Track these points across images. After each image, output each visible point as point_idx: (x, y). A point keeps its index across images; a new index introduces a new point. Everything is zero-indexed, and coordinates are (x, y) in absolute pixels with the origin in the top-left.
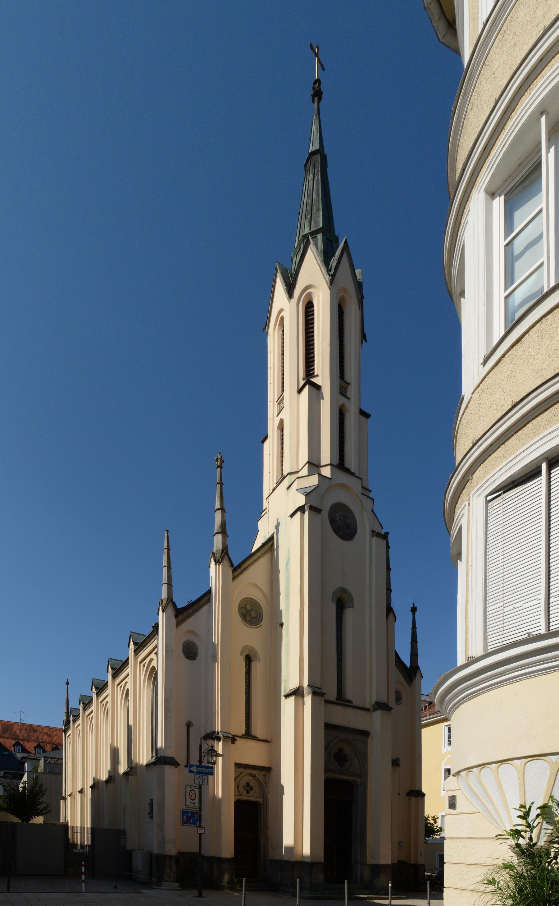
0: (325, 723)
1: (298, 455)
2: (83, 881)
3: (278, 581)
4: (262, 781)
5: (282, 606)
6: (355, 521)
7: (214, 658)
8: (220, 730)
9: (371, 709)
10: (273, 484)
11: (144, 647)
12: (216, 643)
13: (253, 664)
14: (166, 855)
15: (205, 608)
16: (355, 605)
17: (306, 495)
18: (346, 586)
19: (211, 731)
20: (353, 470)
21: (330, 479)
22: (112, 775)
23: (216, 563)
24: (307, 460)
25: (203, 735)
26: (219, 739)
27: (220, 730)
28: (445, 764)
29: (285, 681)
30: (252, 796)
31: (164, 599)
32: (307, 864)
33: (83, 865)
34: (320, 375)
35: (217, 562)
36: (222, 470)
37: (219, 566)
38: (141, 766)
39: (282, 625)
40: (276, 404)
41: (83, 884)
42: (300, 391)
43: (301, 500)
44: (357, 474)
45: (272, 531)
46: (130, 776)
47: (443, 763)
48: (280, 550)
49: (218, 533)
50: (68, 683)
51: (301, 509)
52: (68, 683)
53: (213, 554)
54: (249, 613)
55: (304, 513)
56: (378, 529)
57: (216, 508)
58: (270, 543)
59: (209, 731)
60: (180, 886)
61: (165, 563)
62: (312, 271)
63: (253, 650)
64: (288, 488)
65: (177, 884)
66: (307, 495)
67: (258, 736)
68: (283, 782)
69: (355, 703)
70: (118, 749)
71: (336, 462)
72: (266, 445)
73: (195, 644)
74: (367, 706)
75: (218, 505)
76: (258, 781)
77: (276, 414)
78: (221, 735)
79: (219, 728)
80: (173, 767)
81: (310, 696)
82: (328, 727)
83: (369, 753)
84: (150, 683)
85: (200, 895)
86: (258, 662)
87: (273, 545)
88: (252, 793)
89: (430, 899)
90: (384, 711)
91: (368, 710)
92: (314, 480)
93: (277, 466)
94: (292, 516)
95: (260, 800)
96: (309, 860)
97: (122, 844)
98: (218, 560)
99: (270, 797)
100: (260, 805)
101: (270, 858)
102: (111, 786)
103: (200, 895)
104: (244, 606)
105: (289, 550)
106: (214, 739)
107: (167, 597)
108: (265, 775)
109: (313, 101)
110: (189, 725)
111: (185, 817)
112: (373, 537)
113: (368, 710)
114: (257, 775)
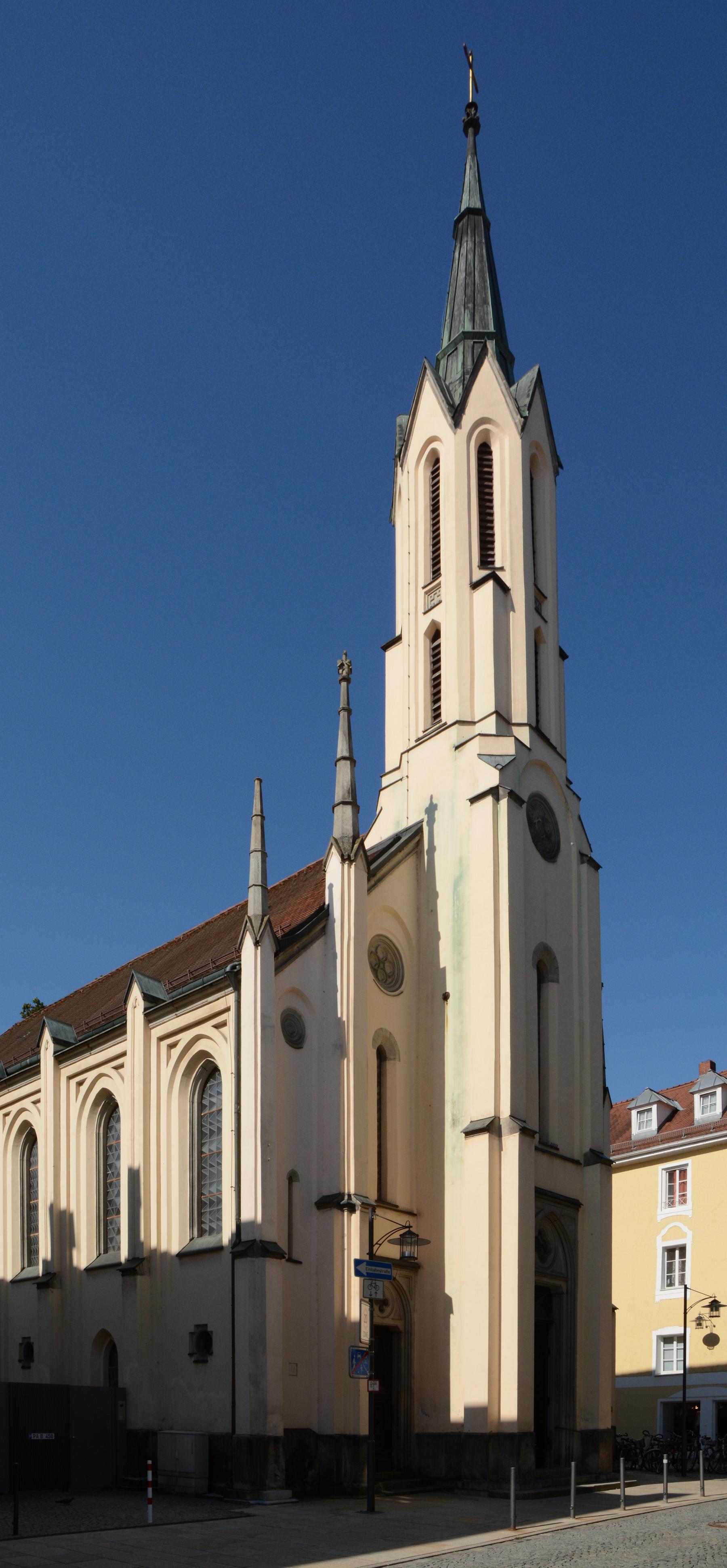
0: (536, 1188)
1: (471, 688)
2: (150, 1501)
3: (433, 912)
4: (405, 1288)
5: (446, 958)
6: (558, 830)
7: (340, 1049)
8: (352, 1191)
9: (582, 1161)
10: (417, 730)
11: (177, 1009)
12: (345, 1019)
13: (389, 1065)
14: (270, 1437)
15: (317, 947)
16: (561, 979)
17: (500, 770)
18: (551, 943)
19: (335, 1192)
20: (553, 741)
21: (529, 749)
22: (55, 1269)
23: (343, 860)
24: (493, 710)
25: (315, 1199)
26: (352, 1209)
27: (352, 1191)
28: (664, 1238)
29: (454, 1103)
30: (387, 1317)
31: (256, 916)
32: (510, 1436)
33: (148, 1467)
34: (507, 568)
35: (345, 858)
36: (350, 686)
37: (349, 867)
38: (165, 1254)
39: (446, 997)
40: (421, 592)
41: (150, 1507)
42: (475, 586)
43: (492, 778)
44: (558, 750)
45: (416, 815)
46: (139, 1277)
48: (437, 855)
49: (344, 803)
51: (493, 792)
53: (336, 840)
54: (382, 965)
55: (497, 799)
56: (586, 851)
57: (339, 756)
58: (417, 839)
59: (326, 1192)
60: (293, 1496)
61: (255, 843)
62: (489, 393)
63: (389, 1038)
64: (457, 748)
65: (288, 1493)
66: (502, 770)
67: (398, 1204)
68: (450, 1288)
69: (562, 1152)
70: (71, 1216)
71: (534, 724)
72: (392, 656)
73: (300, 1016)
74: (577, 1156)
75: (342, 749)
76: (398, 1289)
77: (421, 610)
78: (354, 1200)
79: (350, 1186)
81: (516, 1137)
82: (541, 1194)
83: (579, 1239)
84: (187, 1086)
85: (371, 1509)
86: (397, 1062)
87: (420, 843)
88: (388, 1310)
89: (668, 1481)
90: (604, 1166)
91: (576, 1162)
92: (507, 747)
93: (425, 708)
94: (474, 800)
95: (399, 1324)
96: (515, 1430)
97: (121, 1418)
98: (349, 856)
99: (416, 1317)
100: (399, 1332)
101: (417, 1430)
102: (53, 1294)
103: (371, 1509)
104: (374, 950)
105: (461, 860)
106: (341, 1208)
107: (260, 912)
108: (408, 1278)
109: (466, 132)
110: (292, 1178)
111: (354, 1362)
112: (582, 862)
113: (576, 1162)
114: (397, 1278)
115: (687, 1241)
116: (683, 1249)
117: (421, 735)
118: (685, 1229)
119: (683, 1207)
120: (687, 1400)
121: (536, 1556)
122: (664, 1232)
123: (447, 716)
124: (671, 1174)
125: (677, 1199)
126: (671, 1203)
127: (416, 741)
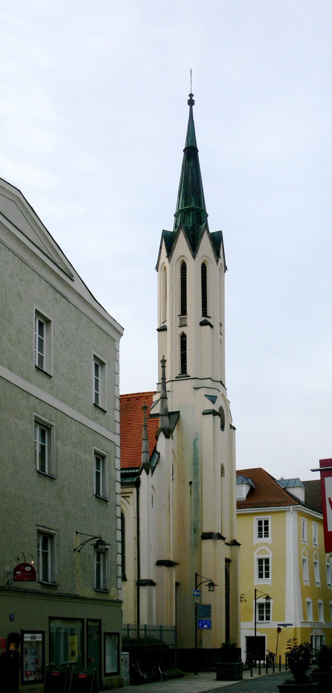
28: (258, 554)
47: (255, 553)
50: (191, 103)
52: (191, 103)
80: (221, 540)
115: (270, 556)
116: (267, 561)
117: (178, 376)
118: (268, 550)
119: (266, 539)
120: (257, 635)
121: (297, 644)
122: (258, 551)
123: (190, 371)
124: (260, 523)
125: (263, 535)
126: (260, 536)
127: (176, 378)
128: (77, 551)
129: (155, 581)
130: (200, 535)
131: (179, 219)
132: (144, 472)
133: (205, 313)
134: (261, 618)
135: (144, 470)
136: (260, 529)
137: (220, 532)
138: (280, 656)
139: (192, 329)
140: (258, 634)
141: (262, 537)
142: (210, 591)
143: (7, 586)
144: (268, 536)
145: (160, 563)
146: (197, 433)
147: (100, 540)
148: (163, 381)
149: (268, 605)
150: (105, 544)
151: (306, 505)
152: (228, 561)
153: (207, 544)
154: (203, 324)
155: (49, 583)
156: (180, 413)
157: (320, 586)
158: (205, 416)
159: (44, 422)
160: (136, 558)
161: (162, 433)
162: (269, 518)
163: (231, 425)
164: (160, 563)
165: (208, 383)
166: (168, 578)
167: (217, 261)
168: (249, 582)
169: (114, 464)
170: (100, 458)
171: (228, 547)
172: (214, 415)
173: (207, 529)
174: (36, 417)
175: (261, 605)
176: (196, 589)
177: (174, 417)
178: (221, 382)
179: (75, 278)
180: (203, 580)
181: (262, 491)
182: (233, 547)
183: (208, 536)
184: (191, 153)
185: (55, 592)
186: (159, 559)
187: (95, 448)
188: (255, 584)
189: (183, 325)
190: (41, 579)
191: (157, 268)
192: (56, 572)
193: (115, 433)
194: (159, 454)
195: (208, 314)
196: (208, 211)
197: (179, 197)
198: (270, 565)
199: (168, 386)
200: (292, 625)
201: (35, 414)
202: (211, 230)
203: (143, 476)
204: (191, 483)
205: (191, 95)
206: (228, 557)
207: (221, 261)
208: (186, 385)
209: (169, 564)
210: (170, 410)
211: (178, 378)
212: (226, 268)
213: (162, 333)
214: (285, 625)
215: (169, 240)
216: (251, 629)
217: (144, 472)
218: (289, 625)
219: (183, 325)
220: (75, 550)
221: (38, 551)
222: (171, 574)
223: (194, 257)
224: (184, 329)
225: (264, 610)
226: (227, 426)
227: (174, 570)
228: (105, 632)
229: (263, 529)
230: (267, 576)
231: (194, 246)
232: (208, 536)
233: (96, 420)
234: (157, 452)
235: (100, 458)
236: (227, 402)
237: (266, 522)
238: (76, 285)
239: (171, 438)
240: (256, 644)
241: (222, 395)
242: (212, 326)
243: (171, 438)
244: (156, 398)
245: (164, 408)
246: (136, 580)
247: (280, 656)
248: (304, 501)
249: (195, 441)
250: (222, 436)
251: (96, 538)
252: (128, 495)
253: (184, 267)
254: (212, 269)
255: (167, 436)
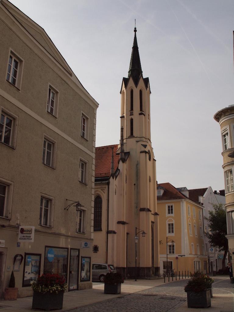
28: (168, 221)
47: (167, 221)
50: (135, 31)
52: (135, 31)
115: (174, 222)
116: (172, 224)
124: (169, 207)
127: (128, 137)
128: (66, 209)
129: (116, 231)
130: (139, 209)
131: (130, 73)
132: (111, 178)
133: (141, 110)
134: (170, 252)
135: (111, 177)
136: (169, 210)
137: (149, 208)
138: (179, 272)
139: (136, 117)
140: (169, 260)
141: (170, 213)
142: (143, 236)
143: (17, 226)
144: (172, 213)
145: (119, 223)
146: (138, 161)
147: (79, 204)
148: (122, 139)
149: (173, 246)
150: (81, 206)
151: (190, 199)
152: (153, 222)
153: (143, 214)
154: (140, 114)
155: (48, 226)
156: (130, 153)
157: (197, 237)
158: (141, 154)
159: (51, 139)
160: (107, 219)
161: (121, 160)
162: (173, 205)
163: (154, 159)
164: (119, 223)
165: (144, 140)
166: (122, 230)
167: (147, 89)
168: (163, 233)
169: (92, 167)
170: (83, 164)
171: (153, 216)
172: (146, 153)
173: (142, 207)
174: (45, 136)
175: (170, 246)
176: (136, 235)
177: (128, 154)
178: (149, 139)
179: (73, 75)
180: (140, 231)
181: (169, 193)
182: (156, 216)
183: (143, 210)
184: (135, 49)
185: (50, 232)
186: (119, 221)
187: (80, 157)
188: (167, 236)
189: (132, 114)
190: (42, 223)
191: (121, 93)
192: (52, 220)
193: (93, 152)
194: (119, 170)
195: (143, 110)
196: (142, 70)
197: (130, 65)
198: (174, 227)
199: (125, 141)
200: (185, 256)
201: (44, 134)
202: (144, 77)
203: (111, 180)
204: (135, 184)
205: (135, 28)
206: (153, 221)
207: (148, 89)
208: (133, 140)
209: (123, 223)
210: (125, 151)
211: (129, 137)
212: (150, 92)
213: (123, 118)
214: (182, 256)
215: (125, 81)
216: (165, 258)
217: (111, 178)
218: (183, 256)
219: (132, 114)
220: (65, 209)
221: (41, 208)
222: (125, 228)
223: (136, 87)
224: (132, 117)
225: (172, 249)
226: (152, 159)
227: (126, 226)
228: (81, 256)
229: (170, 210)
230: (173, 232)
231: (136, 83)
232: (143, 210)
233: (82, 144)
234: (118, 169)
235: (83, 164)
236: (152, 149)
237: (172, 207)
238: (73, 78)
239: (125, 163)
240: (168, 266)
241: (149, 145)
242: (144, 115)
243: (125, 163)
244: (119, 146)
245: (122, 151)
246: (107, 231)
247: (179, 272)
248: (188, 197)
249: (137, 165)
250: (150, 163)
251: (77, 202)
252: (104, 189)
253: (132, 92)
254: (145, 92)
255: (123, 162)
